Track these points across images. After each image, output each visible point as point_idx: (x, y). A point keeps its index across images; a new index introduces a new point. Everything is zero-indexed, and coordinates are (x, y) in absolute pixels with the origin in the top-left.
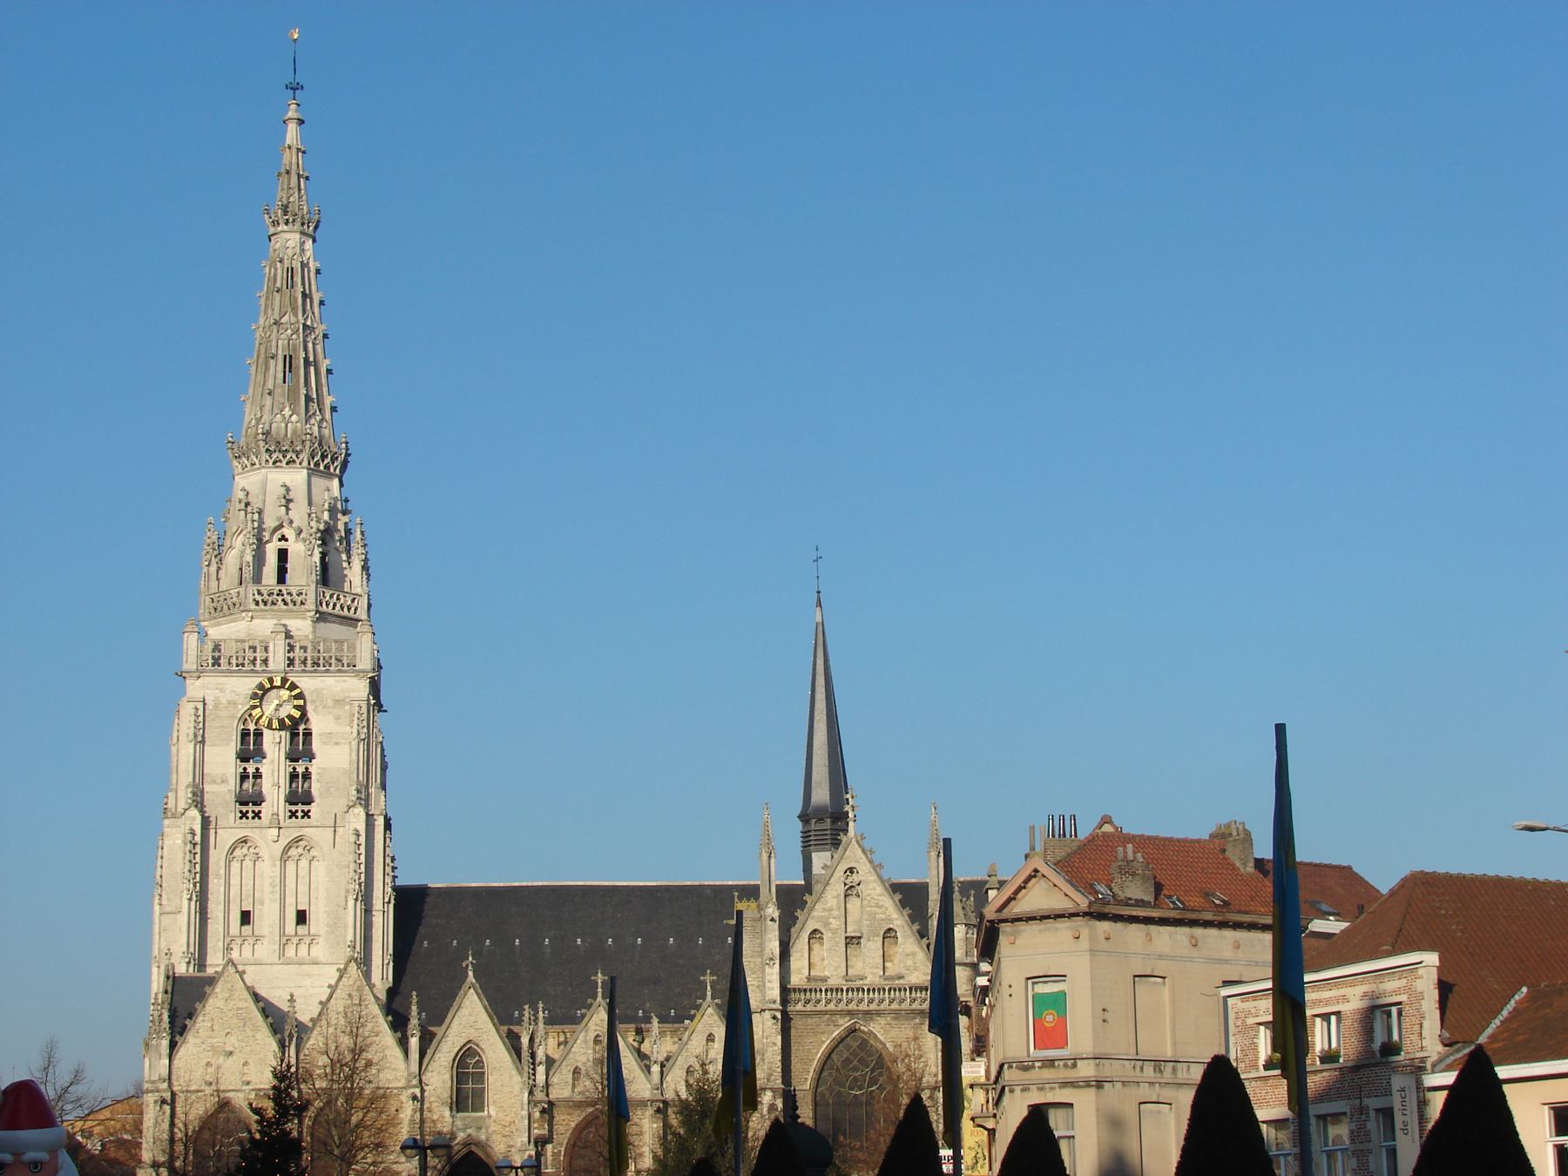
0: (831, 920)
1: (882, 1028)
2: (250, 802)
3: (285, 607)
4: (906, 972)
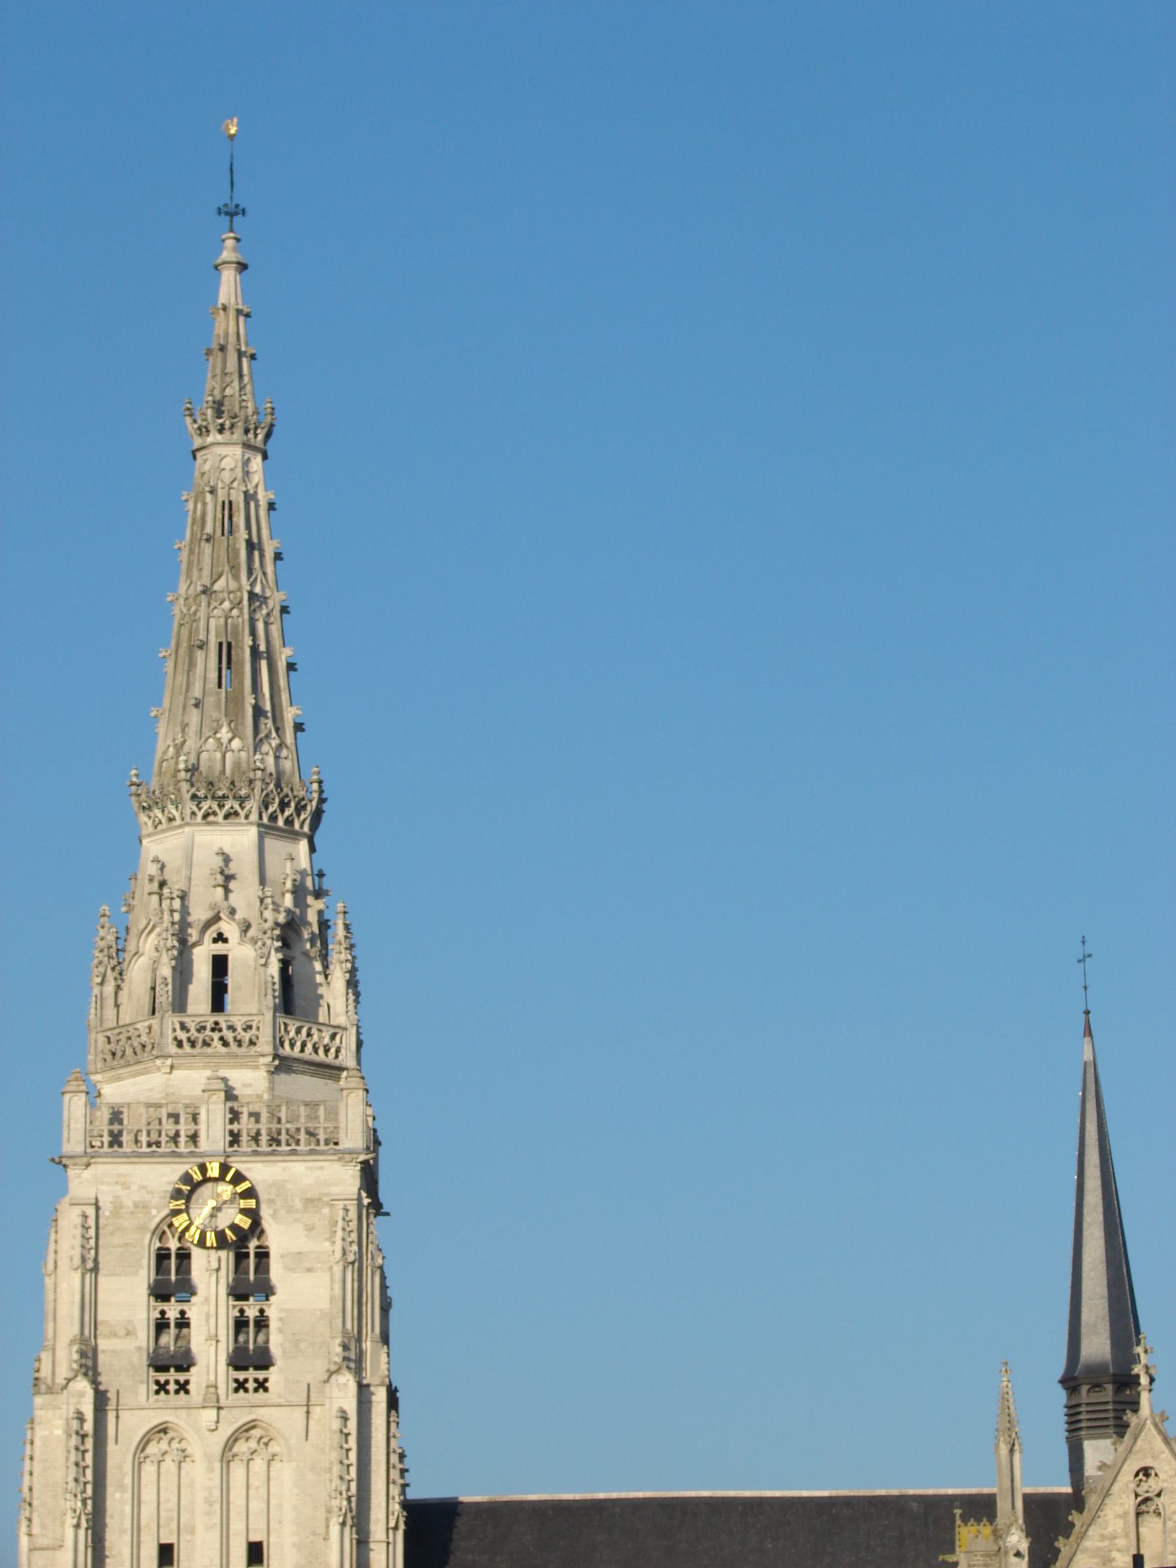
0: (1115, 1554)
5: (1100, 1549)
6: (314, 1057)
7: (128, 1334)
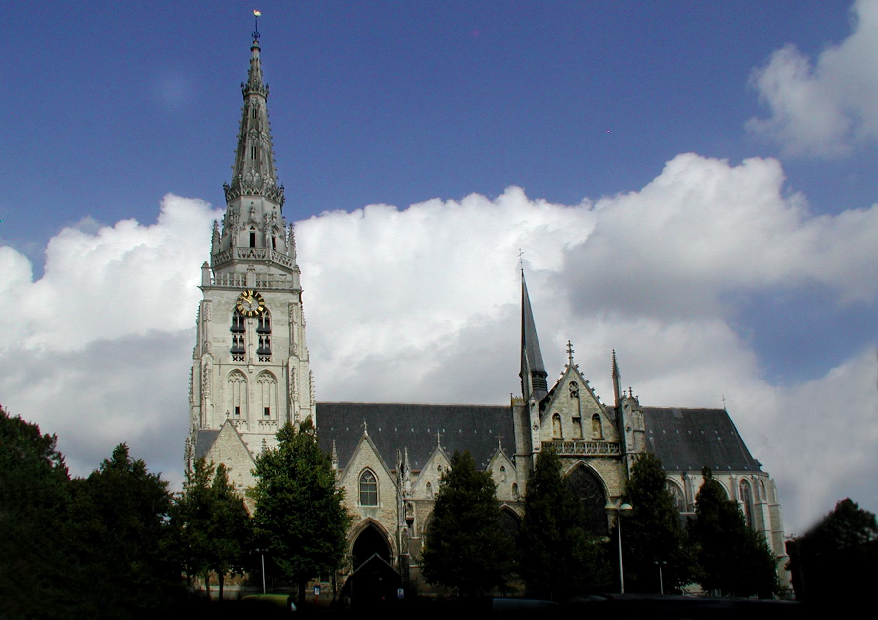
0: (564, 409)
1: (595, 465)
2: (238, 353)
3: (240, 258)
4: (606, 437)
5: (559, 407)
6: (283, 265)
7: (223, 342)
